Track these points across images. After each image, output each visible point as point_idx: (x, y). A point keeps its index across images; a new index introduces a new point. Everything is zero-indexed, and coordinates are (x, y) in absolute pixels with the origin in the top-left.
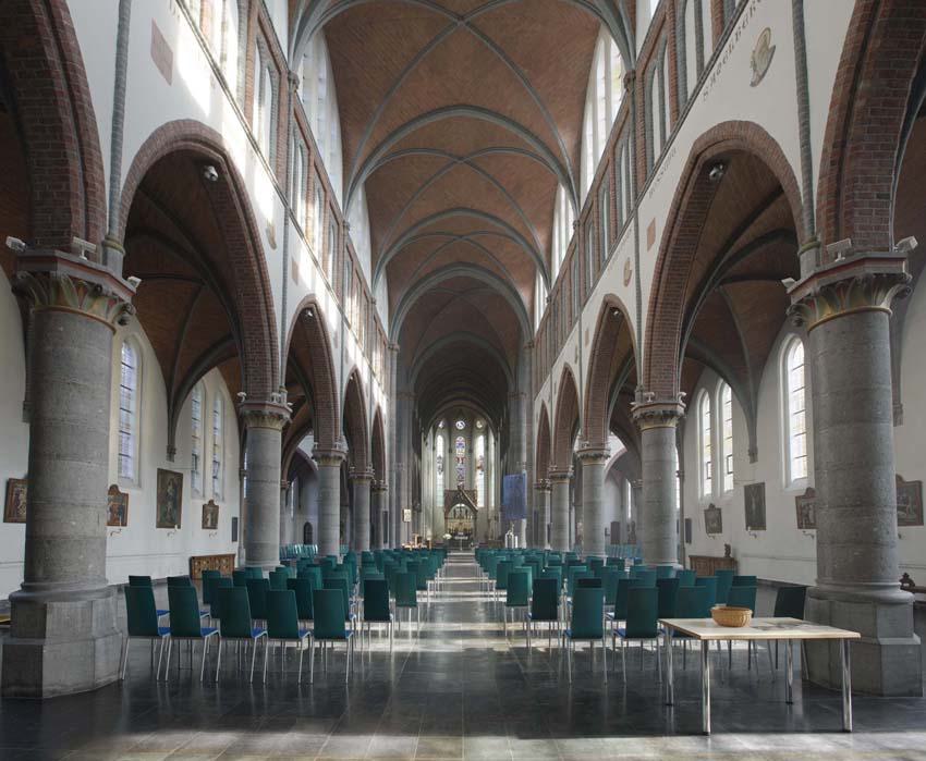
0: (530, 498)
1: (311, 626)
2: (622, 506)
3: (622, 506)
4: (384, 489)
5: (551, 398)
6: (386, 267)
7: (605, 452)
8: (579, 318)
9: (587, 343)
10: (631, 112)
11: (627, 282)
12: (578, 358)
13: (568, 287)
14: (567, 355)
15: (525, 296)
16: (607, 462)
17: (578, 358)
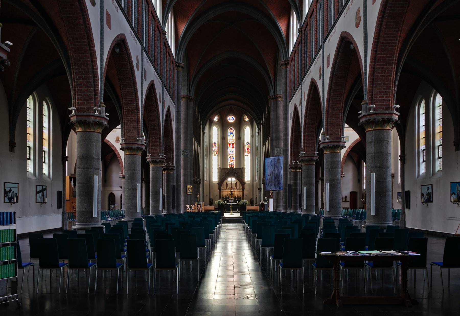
0: (286, 175)
1: (67, 262)
2: (359, 179)
3: (359, 179)
4: (173, 169)
5: (301, 103)
6: (174, 7)
7: (341, 144)
8: (322, 47)
9: (328, 66)
10: (315, 10)
11: (357, 25)
12: (322, 76)
13: (315, 23)
14: (313, 73)
15: (282, 27)
16: (343, 152)
17: (322, 76)
